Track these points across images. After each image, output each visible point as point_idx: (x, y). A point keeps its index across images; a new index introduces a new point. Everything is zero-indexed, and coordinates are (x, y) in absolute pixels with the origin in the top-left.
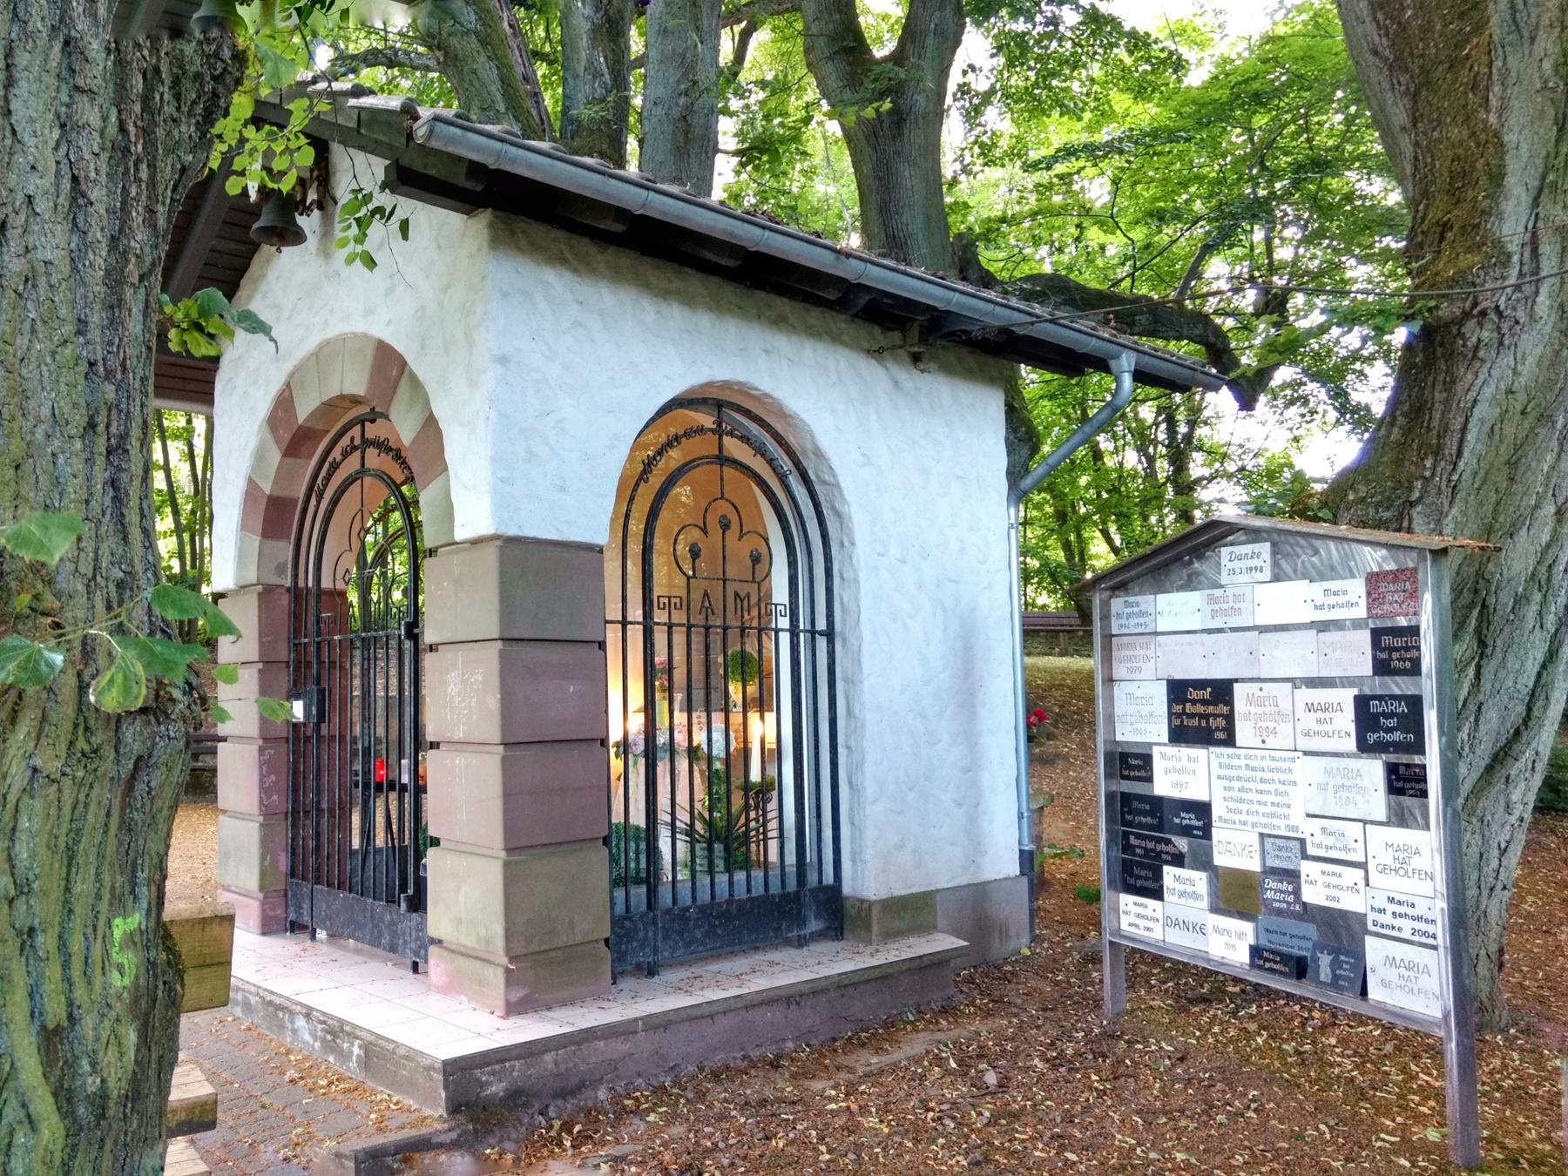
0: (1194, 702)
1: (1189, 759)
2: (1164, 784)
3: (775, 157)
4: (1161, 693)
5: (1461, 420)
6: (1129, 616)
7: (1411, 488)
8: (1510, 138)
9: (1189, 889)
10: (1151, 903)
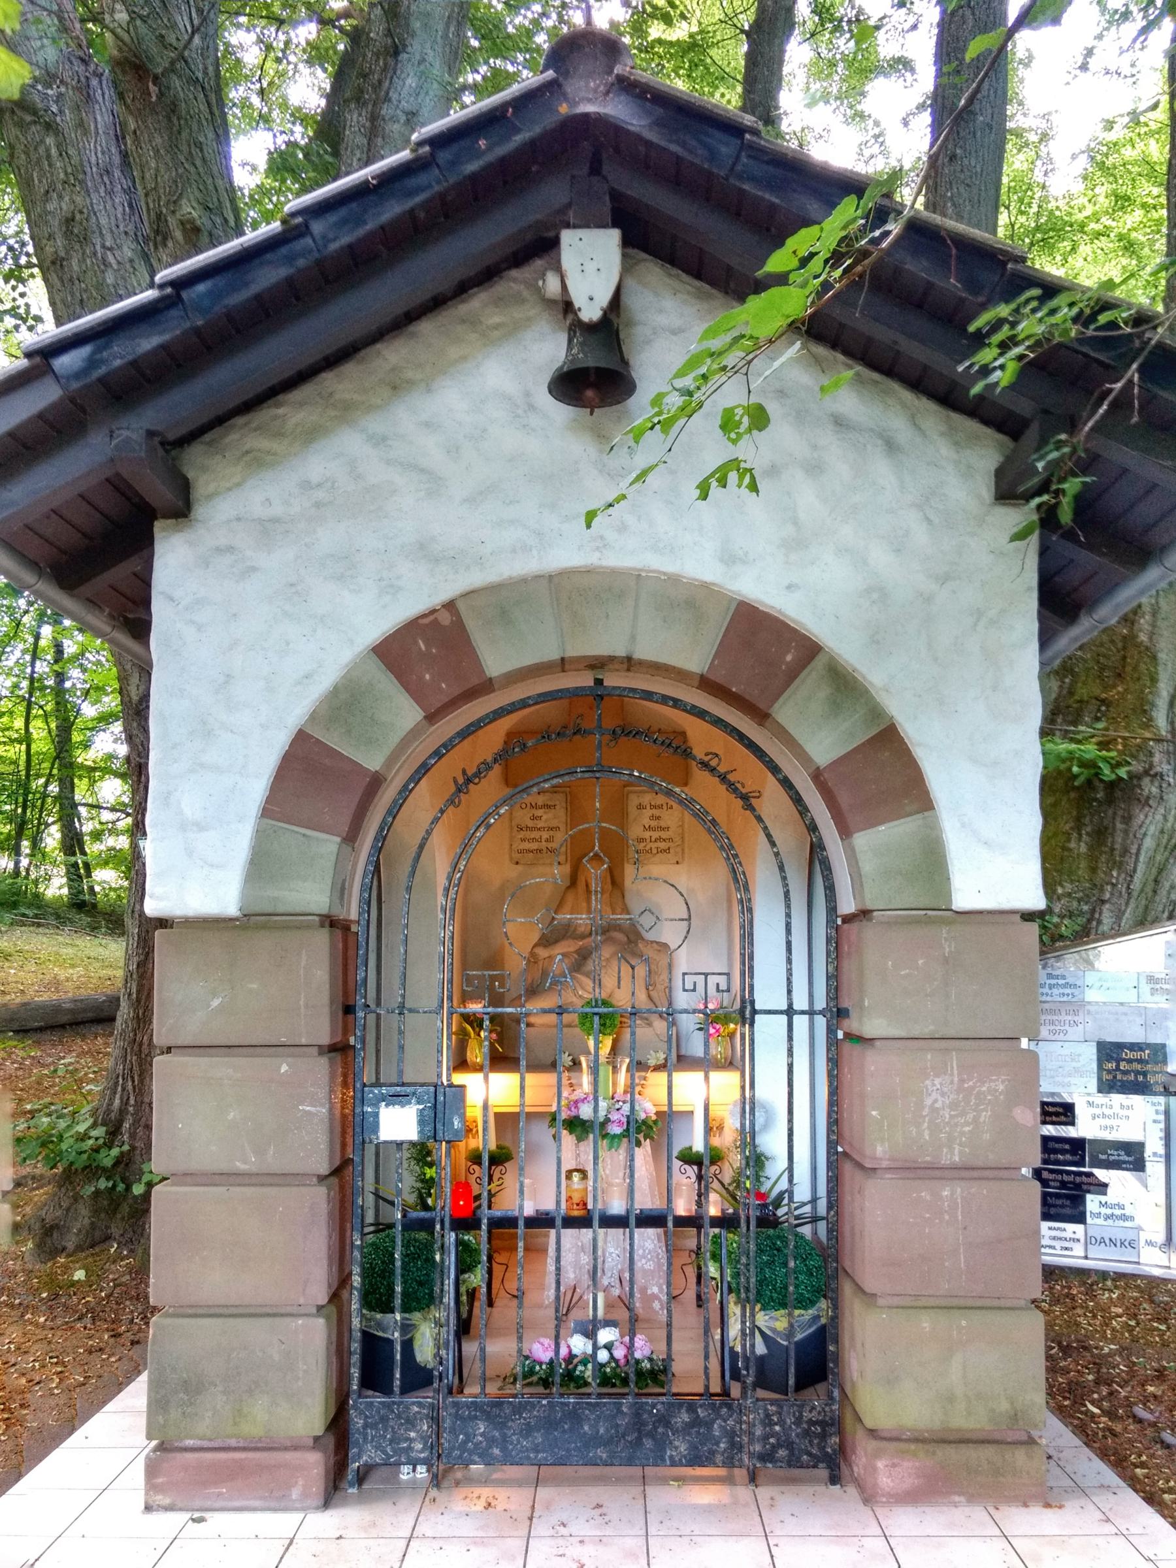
0: (1130, 1061)
1: (1122, 1107)
2: (1085, 1127)
3: (48, 130)
4: (1090, 1054)
5: (1136, 846)
6: (1051, 987)
7: (1102, 890)
8: (1162, 656)
9: (1118, 1212)
10: (1071, 1228)
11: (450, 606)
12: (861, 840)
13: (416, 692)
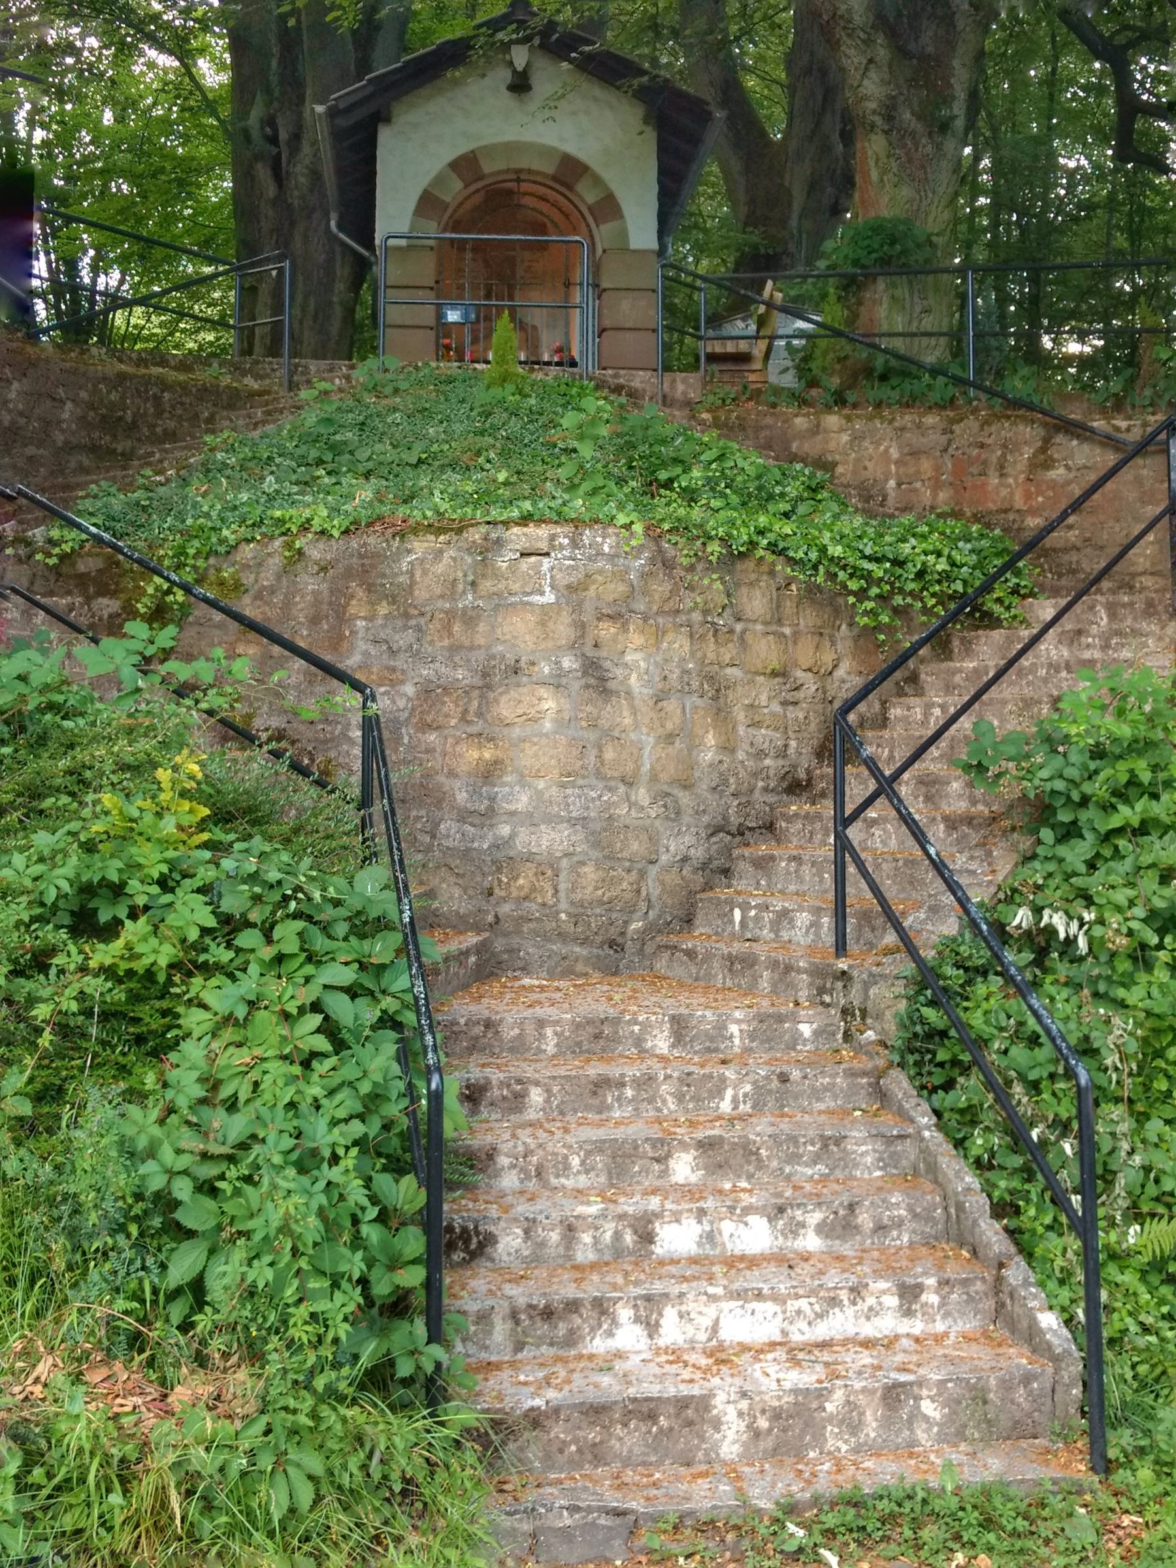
11: (472, 152)
12: (602, 227)
13: (460, 176)
